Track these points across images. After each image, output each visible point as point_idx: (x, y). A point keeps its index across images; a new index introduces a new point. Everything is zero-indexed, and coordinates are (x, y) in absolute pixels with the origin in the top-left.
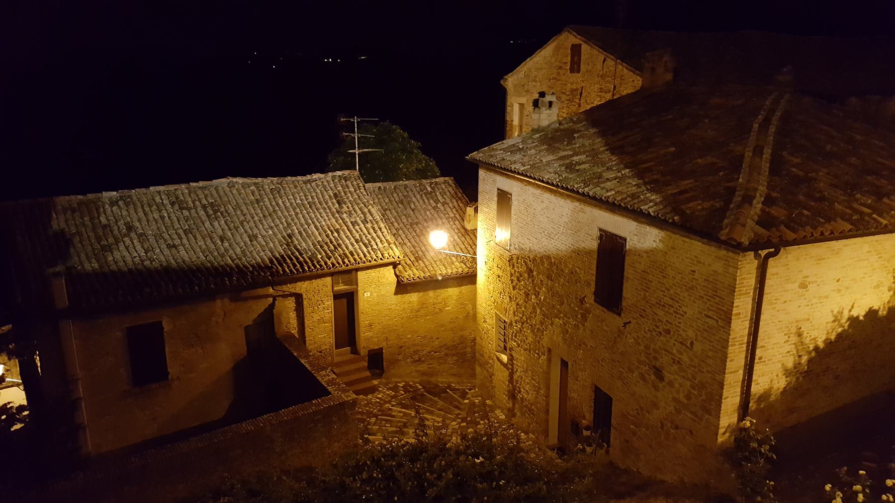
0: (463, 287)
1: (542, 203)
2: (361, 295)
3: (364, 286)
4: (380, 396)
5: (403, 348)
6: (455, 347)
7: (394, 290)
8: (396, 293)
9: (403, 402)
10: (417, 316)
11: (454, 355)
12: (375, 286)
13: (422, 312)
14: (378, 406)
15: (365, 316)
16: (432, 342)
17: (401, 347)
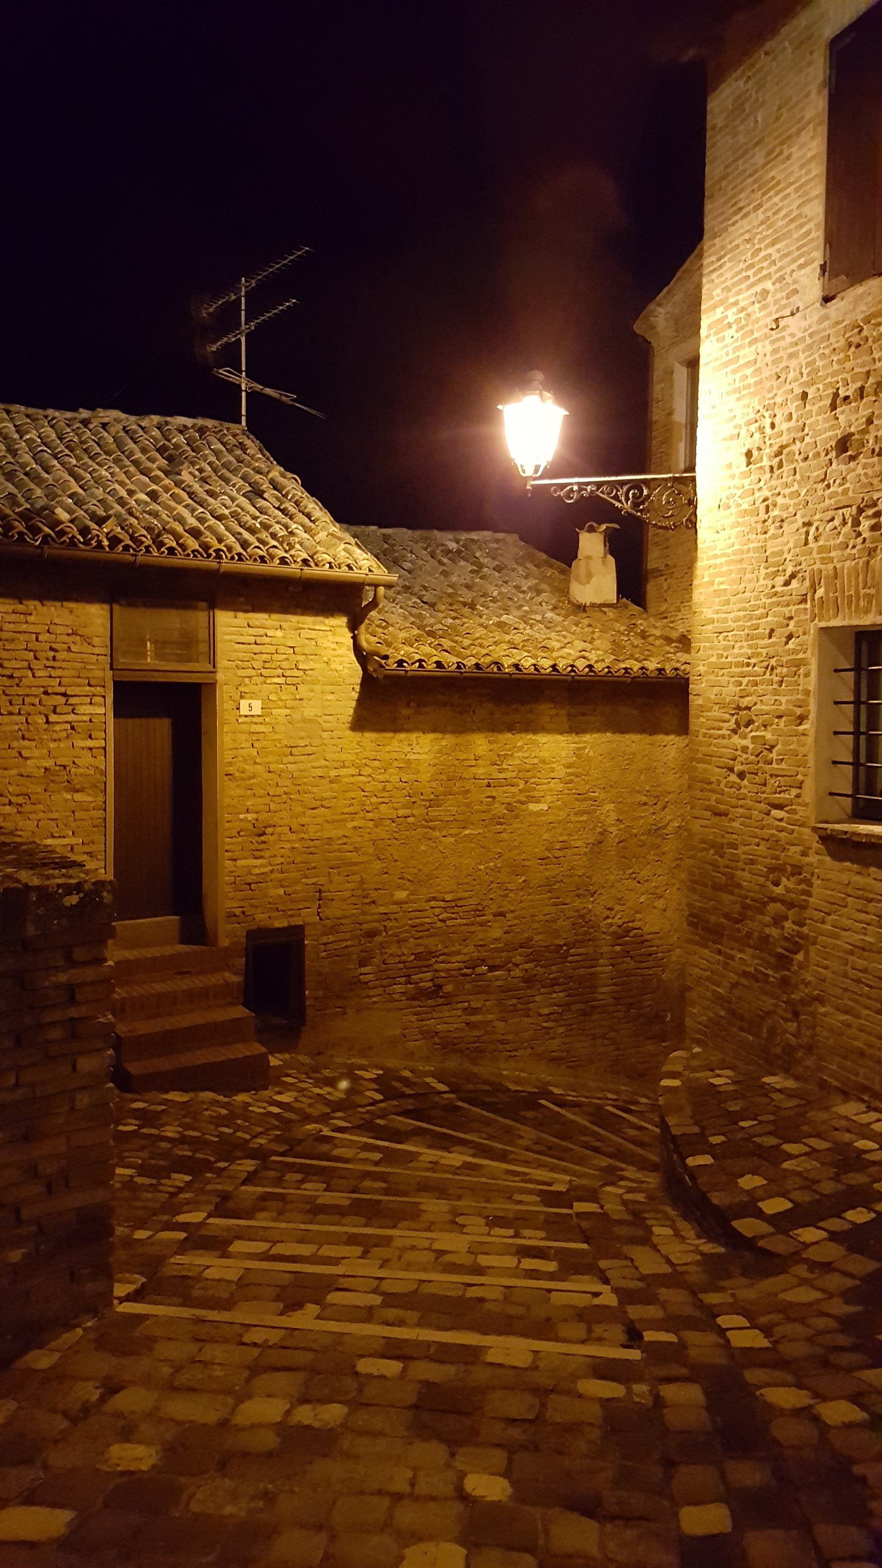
0: (587, 737)
1: (806, 520)
2: (228, 705)
3: (241, 672)
4: (284, 1098)
5: (378, 939)
6: (560, 953)
7: (351, 712)
8: (359, 723)
9: (379, 1121)
10: (428, 823)
11: (554, 983)
12: (281, 680)
13: (450, 807)
14: (276, 1128)
15: (239, 792)
16: (481, 924)
17: (371, 934)
